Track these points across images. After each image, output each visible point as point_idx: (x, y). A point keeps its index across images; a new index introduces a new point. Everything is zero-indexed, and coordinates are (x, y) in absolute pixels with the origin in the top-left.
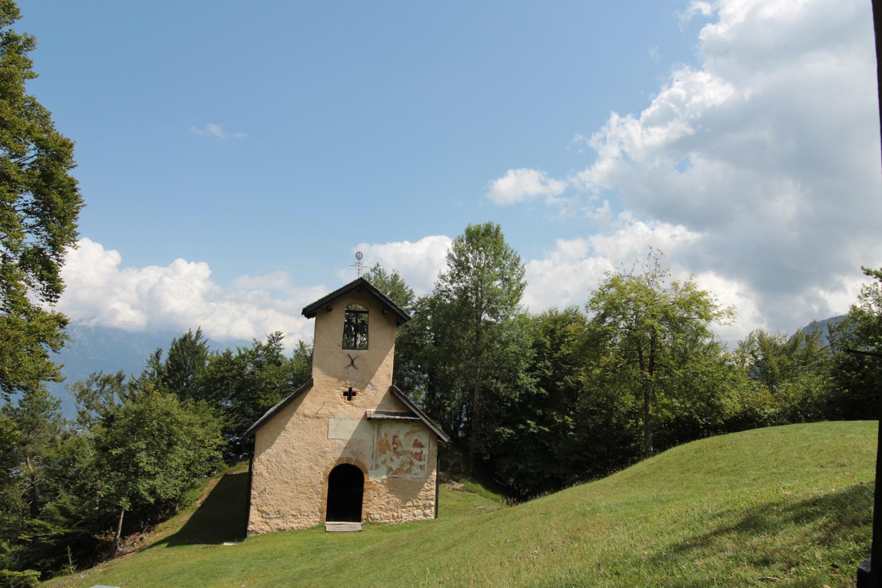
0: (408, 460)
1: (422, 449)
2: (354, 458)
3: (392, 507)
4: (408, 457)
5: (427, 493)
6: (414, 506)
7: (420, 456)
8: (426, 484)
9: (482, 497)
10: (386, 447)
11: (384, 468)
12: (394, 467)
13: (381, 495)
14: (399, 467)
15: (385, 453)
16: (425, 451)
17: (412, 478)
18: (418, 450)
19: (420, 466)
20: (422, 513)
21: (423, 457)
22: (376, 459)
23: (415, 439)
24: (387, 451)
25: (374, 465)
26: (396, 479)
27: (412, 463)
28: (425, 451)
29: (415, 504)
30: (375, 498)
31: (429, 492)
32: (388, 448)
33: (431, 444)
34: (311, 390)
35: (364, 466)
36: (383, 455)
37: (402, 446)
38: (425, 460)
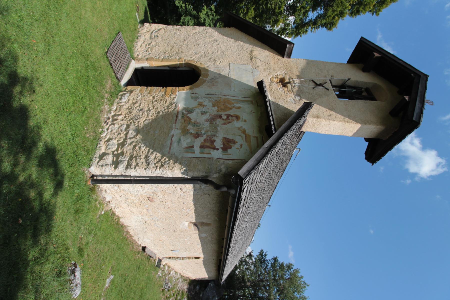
0: (203, 132)
1: (221, 150)
2: (207, 79)
3: (134, 113)
4: (207, 132)
5: (143, 157)
6: (125, 140)
7: (208, 147)
8: (159, 155)
9: (129, 175)
10: (223, 107)
11: (194, 104)
12: (193, 116)
13: (155, 103)
14: (193, 121)
15: (214, 106)
16: (216, 154)
17: (173, 136)
18: (218, 143)
19: (193, 147)
20: (109, 151)
21: (207, 150)
22: (206, 98)
23: (237, 140)
24: (216, 108)
25: (197, 95)
26: (175, 118)
27: (197, 135)
28: (216, 154)
29: (129, 141)
30: (151, 98)
31: (143, 160)
32: (221, 109)
33: (230, 162)
34: (278, 56)
35: (198, 87)
36: (211, 104)
37: (225, 124)
38: (202, 153)
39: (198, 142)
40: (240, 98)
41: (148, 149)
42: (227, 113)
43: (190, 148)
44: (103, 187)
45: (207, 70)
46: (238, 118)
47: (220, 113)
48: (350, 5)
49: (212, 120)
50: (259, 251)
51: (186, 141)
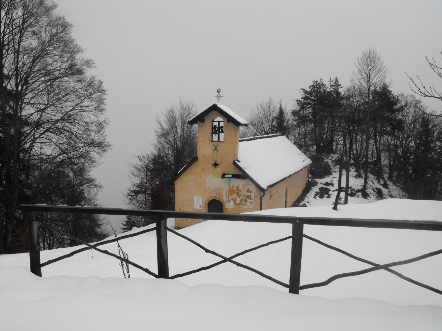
1: (251, 194)
14: (240, 202)
19: (251, 202)
21: (252, 198)
23: (247, 188)
28: (253, 195)
33: (256, 191)
38: (252, 199)
40: (228, 185)
42: (236, 190)
43: (251, 203)
44: (86, 116)
47: (236, 193)
48: (187, 150)
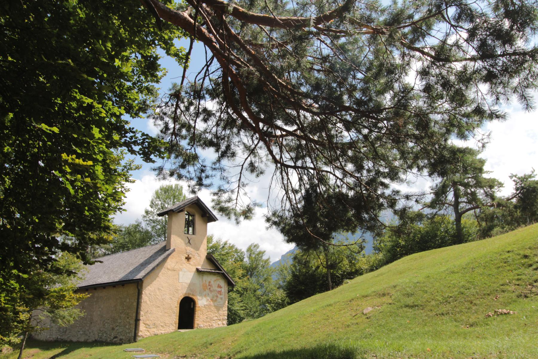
16: (223, 290)
18: (219, 289)
27: (217, 296)
28: (223, 290)
39: (219, 296)
41: (433, 54)
45: (186, 294)
46: (210, 282)
49: (211, 291)
50: (527, 174)
51: (219, 300)
